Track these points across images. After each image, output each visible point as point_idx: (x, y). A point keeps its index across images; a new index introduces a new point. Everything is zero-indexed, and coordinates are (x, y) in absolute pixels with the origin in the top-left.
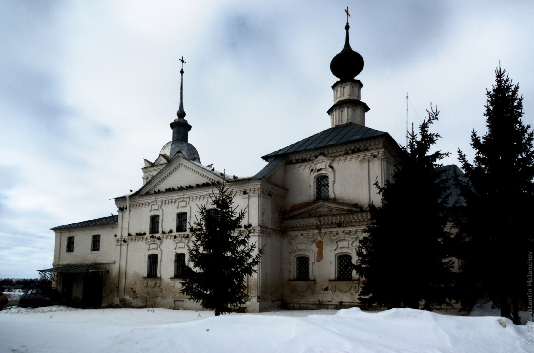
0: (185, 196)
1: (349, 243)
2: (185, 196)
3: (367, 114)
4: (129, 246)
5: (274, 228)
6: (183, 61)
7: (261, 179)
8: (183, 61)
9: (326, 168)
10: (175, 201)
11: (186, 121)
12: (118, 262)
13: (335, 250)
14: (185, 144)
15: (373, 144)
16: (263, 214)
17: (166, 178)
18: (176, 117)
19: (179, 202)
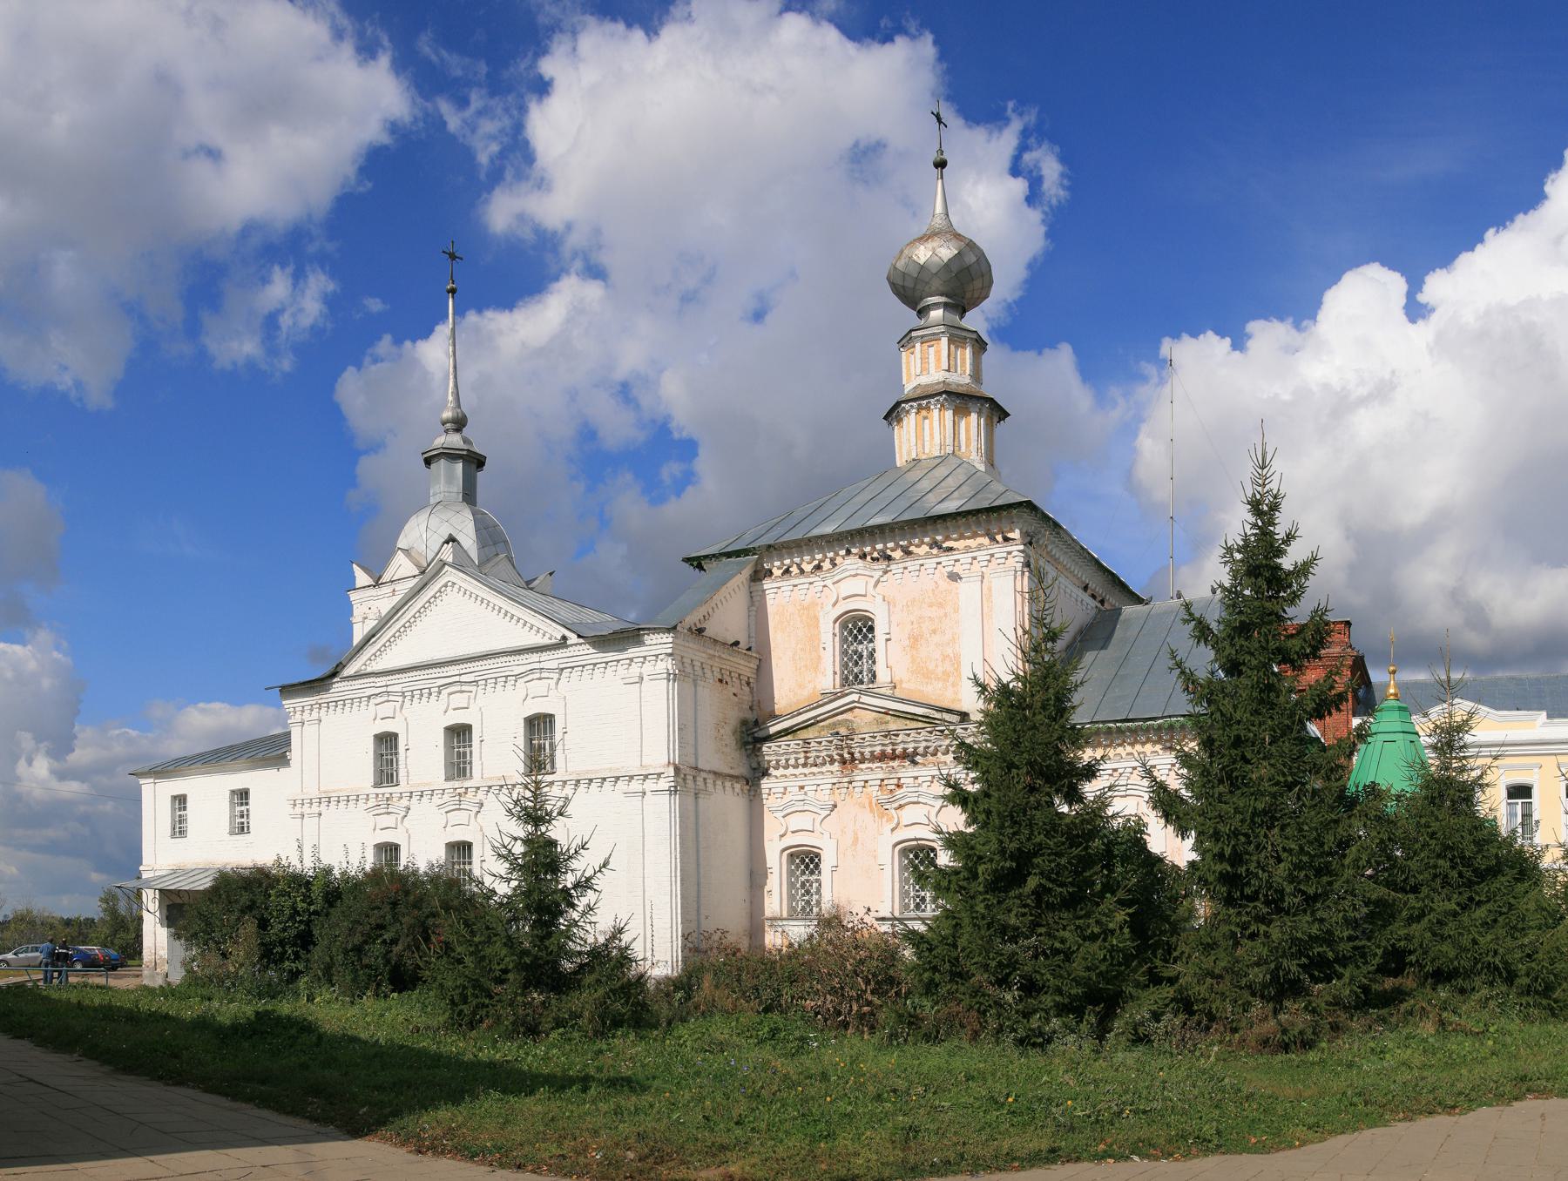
6: (453, 256)
7: (675, 628)
8: (453, 256)
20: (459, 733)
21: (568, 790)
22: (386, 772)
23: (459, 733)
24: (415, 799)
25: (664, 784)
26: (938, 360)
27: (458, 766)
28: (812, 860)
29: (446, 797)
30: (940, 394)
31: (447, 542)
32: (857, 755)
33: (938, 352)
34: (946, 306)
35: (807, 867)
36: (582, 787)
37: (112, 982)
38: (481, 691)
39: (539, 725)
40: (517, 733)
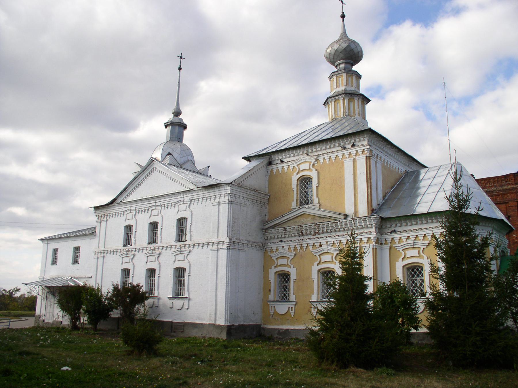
0: (157, 204)
1: (332, 257)
2: (157, 204)
3: (368, 106)
4: (105, 259)
5: (507, 232)
6: (181, 58)
7: (231, 183)
8: (181, 58)
9: (310, 169)
10: (148, 209)
11: (181, 119)
12: (94, 277)
13: (318, 264)
14: (178, 145)
15: (328, 147)
16: (234, 222)
17: (140, 184)
18: (172, 116)
19: (152, 210)
20: (154, 225)
21: (160, 250)
22: (128, 241)
23: (154, 225)
24: (137, 252)
25: (225, 246)
26: (342, 82)
27: (153, 239)
28: (287, 277)
29: (148, 251)
30: (343, 94)
31: (168, 155)
32: (304, 233)
33: (342, 80)
34: (346, 63)
35: (285, 280)
36: (196, 247)
37: (503, 218)
38: (163, 209)
39: (181, 222)
40: (174, 224)
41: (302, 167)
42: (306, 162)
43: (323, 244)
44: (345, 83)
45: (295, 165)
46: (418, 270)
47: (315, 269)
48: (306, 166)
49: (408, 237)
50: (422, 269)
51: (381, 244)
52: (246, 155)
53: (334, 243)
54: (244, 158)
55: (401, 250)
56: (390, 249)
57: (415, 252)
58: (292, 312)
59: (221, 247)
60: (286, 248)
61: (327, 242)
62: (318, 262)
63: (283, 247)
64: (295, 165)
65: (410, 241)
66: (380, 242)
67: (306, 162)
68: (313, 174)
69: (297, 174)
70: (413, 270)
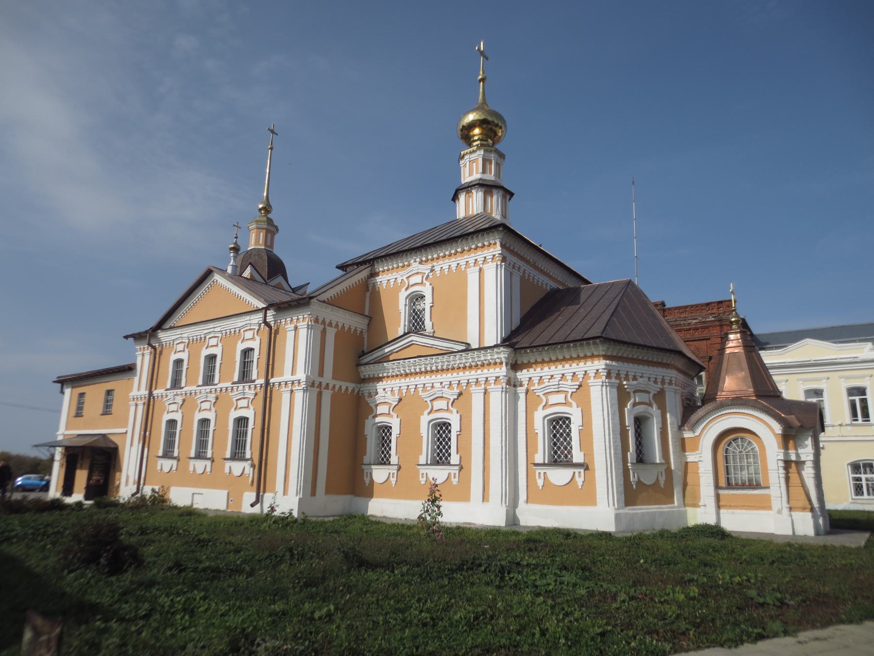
2: (216, 330)
41: (413, 280)
42: (417, 273)
43: (437, 385)
44: (480, 170)
45: (404, 278)
46: (564, 423)
47: (425, 419)
48: (417, 279)
49: (552, 376)
50: (570, 422)
51: (515, 386)
52: (340, 262)
53: (450, 384)
54: (338, 267)
55: (541, 394)
56: (527, 393)
57: (560, 398)
58: (455, 481)
59: (297, 388)
60: (388, 390)
61: (441, 383)
62: (429, 410)
63: (384, 389)
64: (404, 278)
65: (555, 381)
66: (512, 383)
67: (417, 273)
68: (427, 291)
69: (407, 289)
70: (558, 423)
